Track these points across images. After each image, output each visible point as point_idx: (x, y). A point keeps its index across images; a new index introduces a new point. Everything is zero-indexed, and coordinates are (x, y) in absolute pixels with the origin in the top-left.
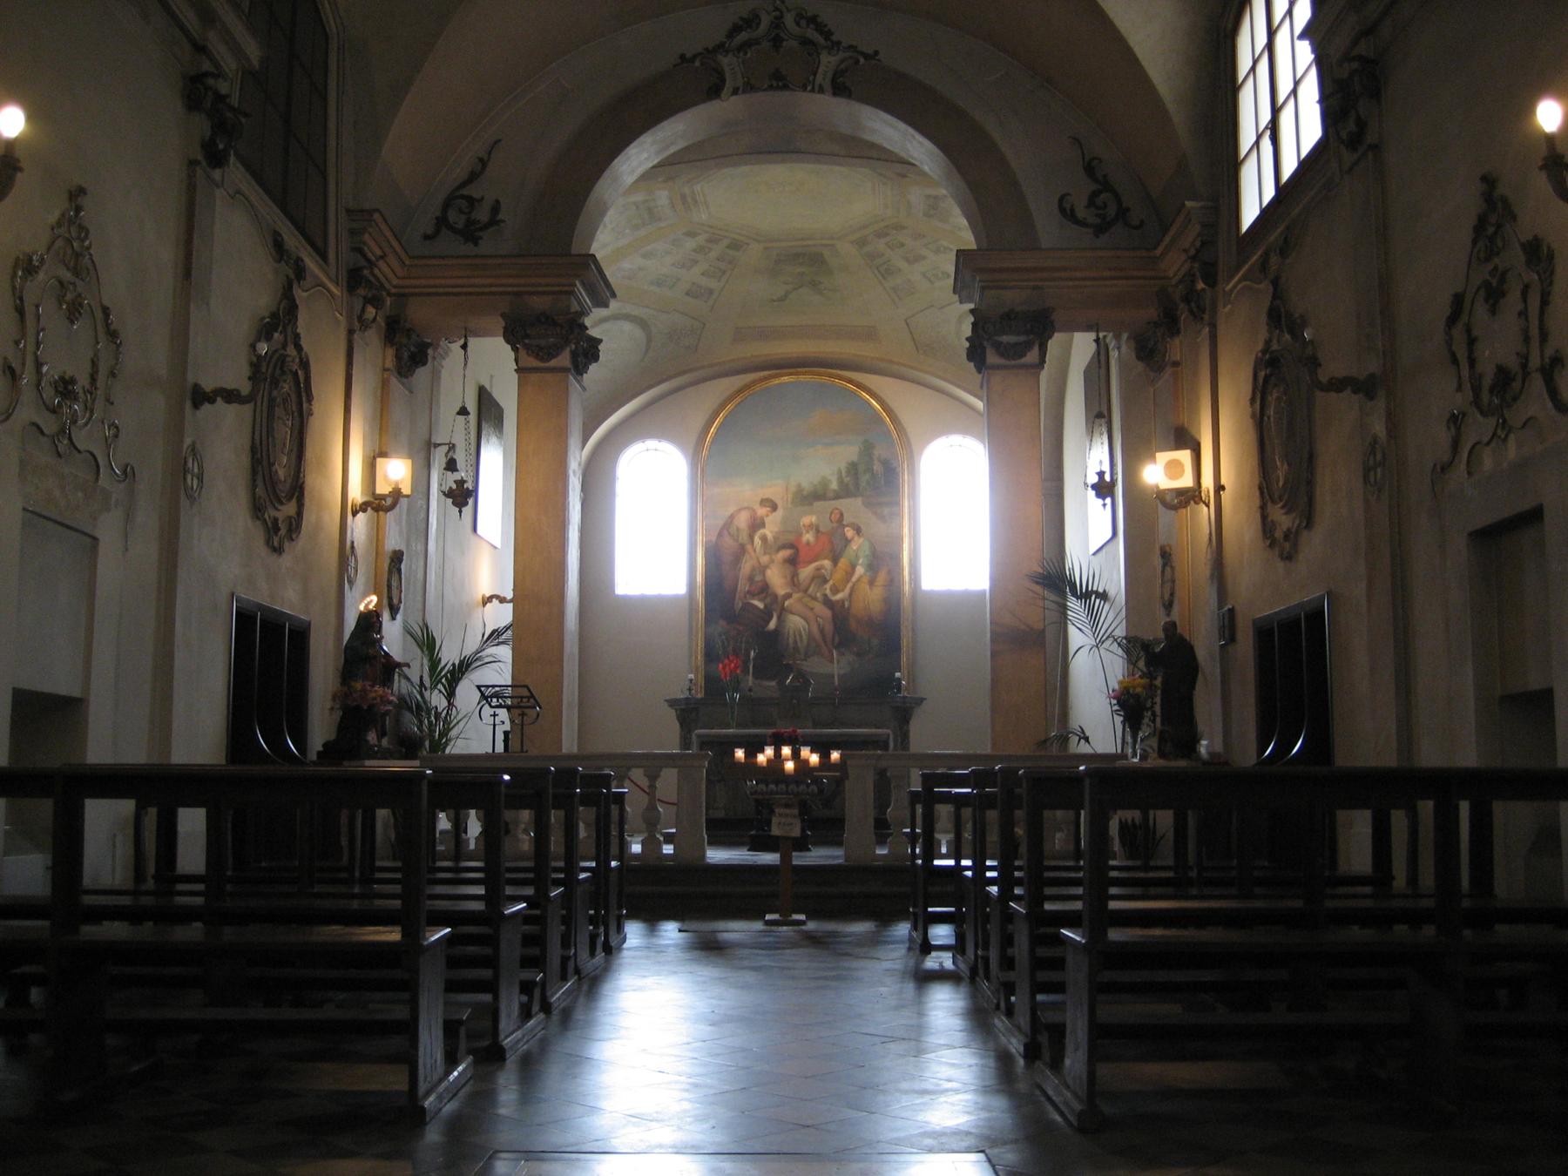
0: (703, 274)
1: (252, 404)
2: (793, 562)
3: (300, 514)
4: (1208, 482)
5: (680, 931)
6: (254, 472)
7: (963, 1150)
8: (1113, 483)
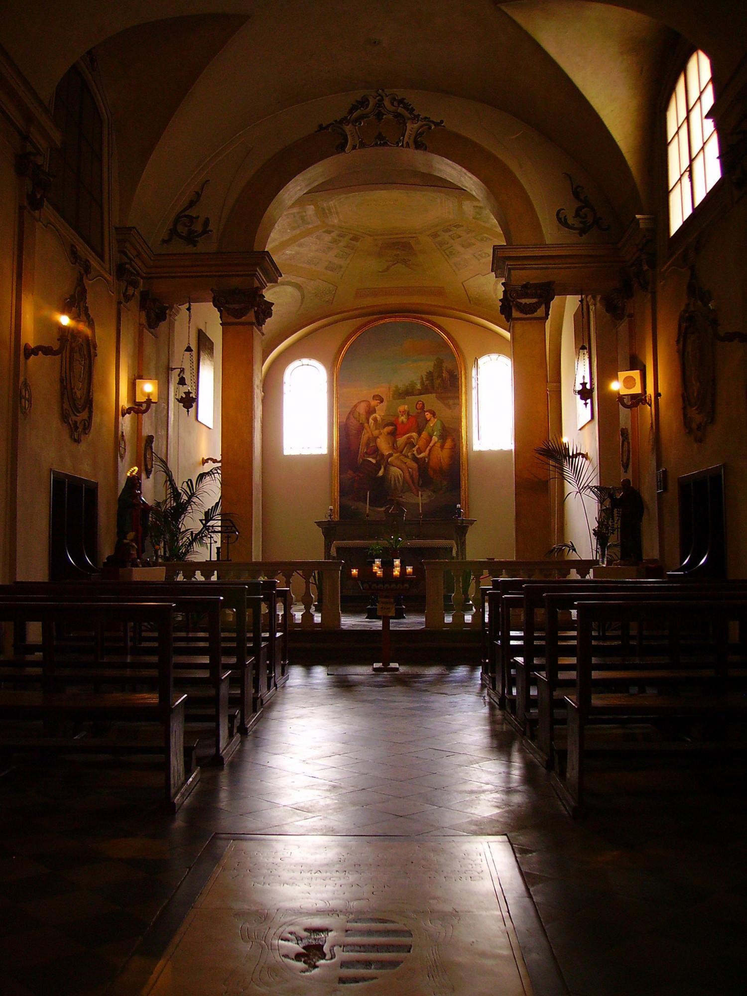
0: (336, 256)
1: (60, 355)
2: (393, 434)
3: (90, 417)
4: (650, 390)
5: (328, 675)
6: (62, 394)
7: (494, 833)
8: (592, 389)
